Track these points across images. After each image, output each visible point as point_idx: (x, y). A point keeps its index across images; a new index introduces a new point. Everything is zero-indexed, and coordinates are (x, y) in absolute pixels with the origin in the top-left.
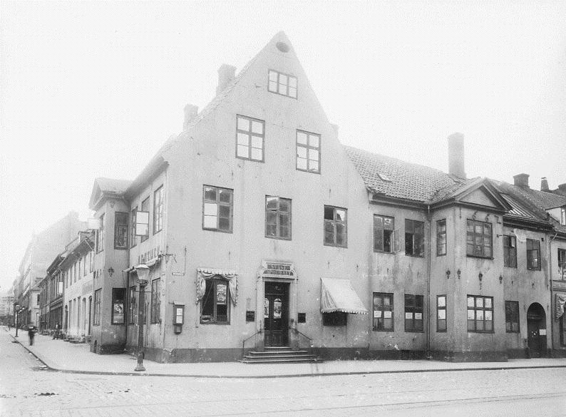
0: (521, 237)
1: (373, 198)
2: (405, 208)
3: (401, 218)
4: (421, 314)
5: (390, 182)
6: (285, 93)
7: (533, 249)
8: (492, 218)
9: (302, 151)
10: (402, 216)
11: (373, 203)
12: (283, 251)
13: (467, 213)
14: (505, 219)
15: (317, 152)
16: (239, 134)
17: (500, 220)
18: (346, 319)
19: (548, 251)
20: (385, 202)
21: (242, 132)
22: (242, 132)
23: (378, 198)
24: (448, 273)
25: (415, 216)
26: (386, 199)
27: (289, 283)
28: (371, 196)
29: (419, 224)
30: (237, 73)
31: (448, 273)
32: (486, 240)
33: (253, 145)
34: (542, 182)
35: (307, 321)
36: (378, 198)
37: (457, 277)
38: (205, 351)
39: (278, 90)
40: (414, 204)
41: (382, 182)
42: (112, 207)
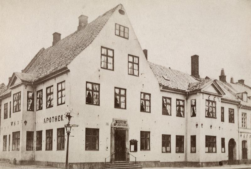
0: (227, 107)
5: (169, 80)
6: (123, 36)
7: (231, 112)
8: (217, 99)
9: (104, 58)
10: (174, 97)
11: (161, 91)
12: (119, 114)
13: (206, 97)
14: (222, 99)
16: (108, 57)
19: (148, 143)
20: (175, 92)
23: (165, 88)
24: (197, 125)
25: (181, 97)
28: (162, 87)
31: (197, 125)
32: (214, 108)
33: (109, 61)
34: (222, 70)
36: (165, 88)
38: (233, 117)
39: (120, 35)
40: (172, 90)
41: (165, 80)
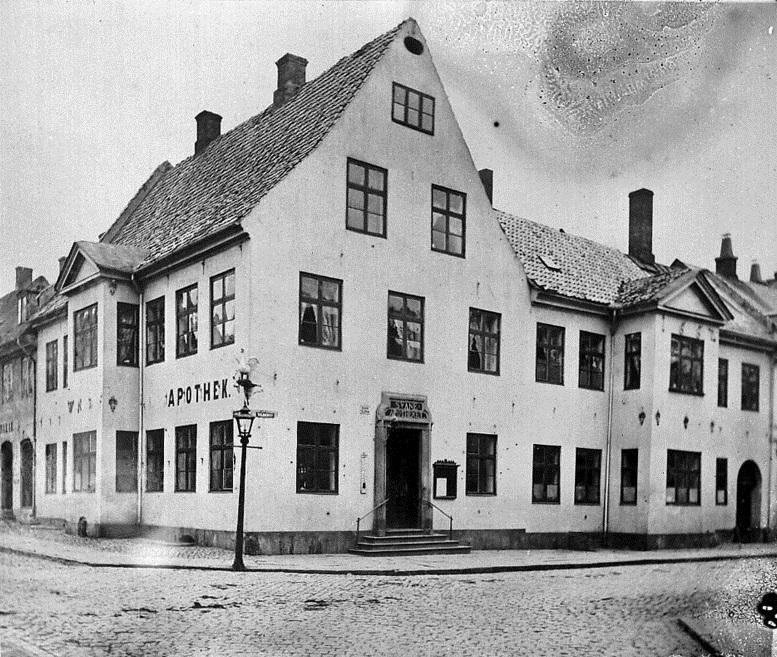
1: (538, 298)
2: (743, 347)
3: (573, 329)
4: (445, 495)
5: (558, 270)
11: (534, 304)
14: (723, 334)
15: (381, 198)
17: (717, 336)
18: (722, 459)
21: (377, 193)
22: (377, 193)
24: (642, 416)
25: (594, 326)
26: (590, 307)
27: (421, 430)
29: (597, 339)
30: (311, 74)
31: (642, 416)
35: (727, 456)
36: (543, 297)
37: (654, 421)
41: (547, 270)
42: (112, 293)
